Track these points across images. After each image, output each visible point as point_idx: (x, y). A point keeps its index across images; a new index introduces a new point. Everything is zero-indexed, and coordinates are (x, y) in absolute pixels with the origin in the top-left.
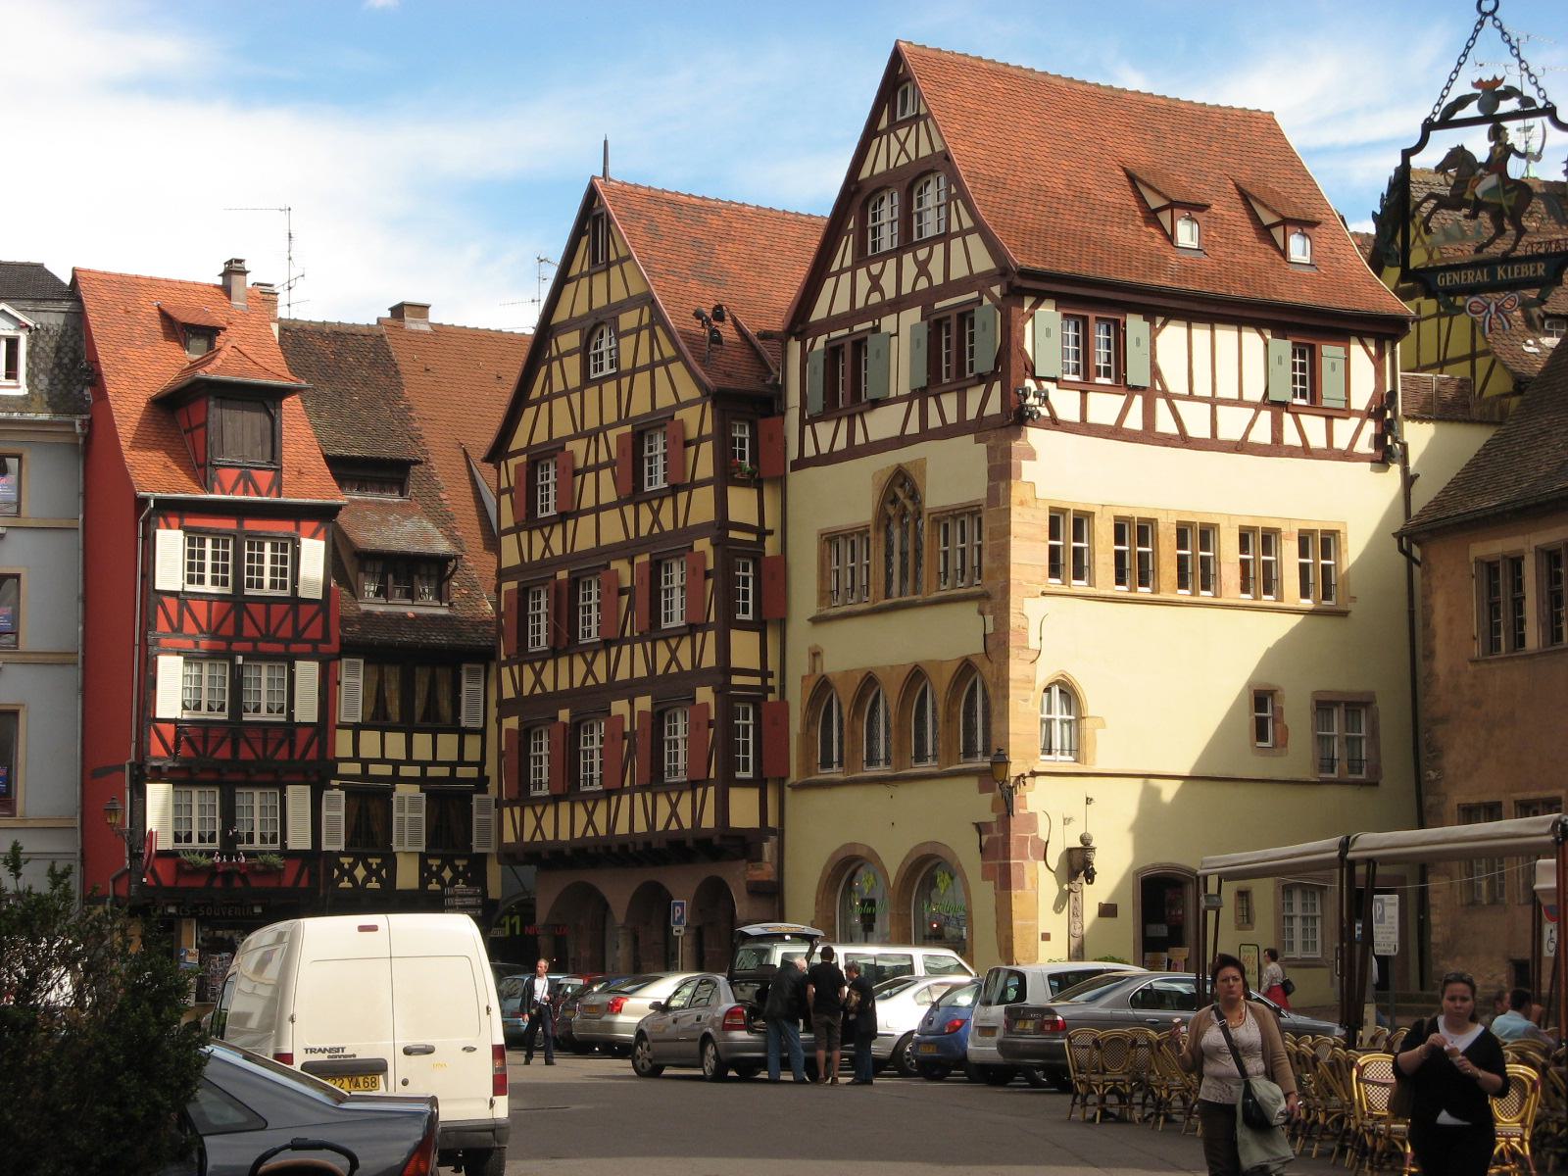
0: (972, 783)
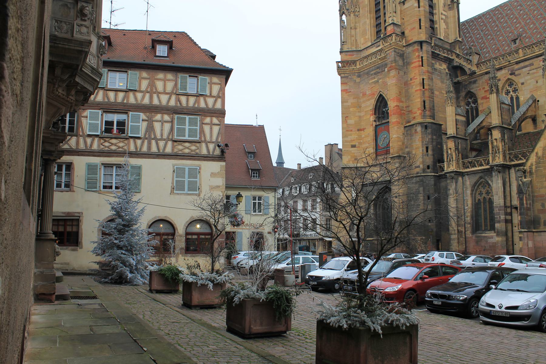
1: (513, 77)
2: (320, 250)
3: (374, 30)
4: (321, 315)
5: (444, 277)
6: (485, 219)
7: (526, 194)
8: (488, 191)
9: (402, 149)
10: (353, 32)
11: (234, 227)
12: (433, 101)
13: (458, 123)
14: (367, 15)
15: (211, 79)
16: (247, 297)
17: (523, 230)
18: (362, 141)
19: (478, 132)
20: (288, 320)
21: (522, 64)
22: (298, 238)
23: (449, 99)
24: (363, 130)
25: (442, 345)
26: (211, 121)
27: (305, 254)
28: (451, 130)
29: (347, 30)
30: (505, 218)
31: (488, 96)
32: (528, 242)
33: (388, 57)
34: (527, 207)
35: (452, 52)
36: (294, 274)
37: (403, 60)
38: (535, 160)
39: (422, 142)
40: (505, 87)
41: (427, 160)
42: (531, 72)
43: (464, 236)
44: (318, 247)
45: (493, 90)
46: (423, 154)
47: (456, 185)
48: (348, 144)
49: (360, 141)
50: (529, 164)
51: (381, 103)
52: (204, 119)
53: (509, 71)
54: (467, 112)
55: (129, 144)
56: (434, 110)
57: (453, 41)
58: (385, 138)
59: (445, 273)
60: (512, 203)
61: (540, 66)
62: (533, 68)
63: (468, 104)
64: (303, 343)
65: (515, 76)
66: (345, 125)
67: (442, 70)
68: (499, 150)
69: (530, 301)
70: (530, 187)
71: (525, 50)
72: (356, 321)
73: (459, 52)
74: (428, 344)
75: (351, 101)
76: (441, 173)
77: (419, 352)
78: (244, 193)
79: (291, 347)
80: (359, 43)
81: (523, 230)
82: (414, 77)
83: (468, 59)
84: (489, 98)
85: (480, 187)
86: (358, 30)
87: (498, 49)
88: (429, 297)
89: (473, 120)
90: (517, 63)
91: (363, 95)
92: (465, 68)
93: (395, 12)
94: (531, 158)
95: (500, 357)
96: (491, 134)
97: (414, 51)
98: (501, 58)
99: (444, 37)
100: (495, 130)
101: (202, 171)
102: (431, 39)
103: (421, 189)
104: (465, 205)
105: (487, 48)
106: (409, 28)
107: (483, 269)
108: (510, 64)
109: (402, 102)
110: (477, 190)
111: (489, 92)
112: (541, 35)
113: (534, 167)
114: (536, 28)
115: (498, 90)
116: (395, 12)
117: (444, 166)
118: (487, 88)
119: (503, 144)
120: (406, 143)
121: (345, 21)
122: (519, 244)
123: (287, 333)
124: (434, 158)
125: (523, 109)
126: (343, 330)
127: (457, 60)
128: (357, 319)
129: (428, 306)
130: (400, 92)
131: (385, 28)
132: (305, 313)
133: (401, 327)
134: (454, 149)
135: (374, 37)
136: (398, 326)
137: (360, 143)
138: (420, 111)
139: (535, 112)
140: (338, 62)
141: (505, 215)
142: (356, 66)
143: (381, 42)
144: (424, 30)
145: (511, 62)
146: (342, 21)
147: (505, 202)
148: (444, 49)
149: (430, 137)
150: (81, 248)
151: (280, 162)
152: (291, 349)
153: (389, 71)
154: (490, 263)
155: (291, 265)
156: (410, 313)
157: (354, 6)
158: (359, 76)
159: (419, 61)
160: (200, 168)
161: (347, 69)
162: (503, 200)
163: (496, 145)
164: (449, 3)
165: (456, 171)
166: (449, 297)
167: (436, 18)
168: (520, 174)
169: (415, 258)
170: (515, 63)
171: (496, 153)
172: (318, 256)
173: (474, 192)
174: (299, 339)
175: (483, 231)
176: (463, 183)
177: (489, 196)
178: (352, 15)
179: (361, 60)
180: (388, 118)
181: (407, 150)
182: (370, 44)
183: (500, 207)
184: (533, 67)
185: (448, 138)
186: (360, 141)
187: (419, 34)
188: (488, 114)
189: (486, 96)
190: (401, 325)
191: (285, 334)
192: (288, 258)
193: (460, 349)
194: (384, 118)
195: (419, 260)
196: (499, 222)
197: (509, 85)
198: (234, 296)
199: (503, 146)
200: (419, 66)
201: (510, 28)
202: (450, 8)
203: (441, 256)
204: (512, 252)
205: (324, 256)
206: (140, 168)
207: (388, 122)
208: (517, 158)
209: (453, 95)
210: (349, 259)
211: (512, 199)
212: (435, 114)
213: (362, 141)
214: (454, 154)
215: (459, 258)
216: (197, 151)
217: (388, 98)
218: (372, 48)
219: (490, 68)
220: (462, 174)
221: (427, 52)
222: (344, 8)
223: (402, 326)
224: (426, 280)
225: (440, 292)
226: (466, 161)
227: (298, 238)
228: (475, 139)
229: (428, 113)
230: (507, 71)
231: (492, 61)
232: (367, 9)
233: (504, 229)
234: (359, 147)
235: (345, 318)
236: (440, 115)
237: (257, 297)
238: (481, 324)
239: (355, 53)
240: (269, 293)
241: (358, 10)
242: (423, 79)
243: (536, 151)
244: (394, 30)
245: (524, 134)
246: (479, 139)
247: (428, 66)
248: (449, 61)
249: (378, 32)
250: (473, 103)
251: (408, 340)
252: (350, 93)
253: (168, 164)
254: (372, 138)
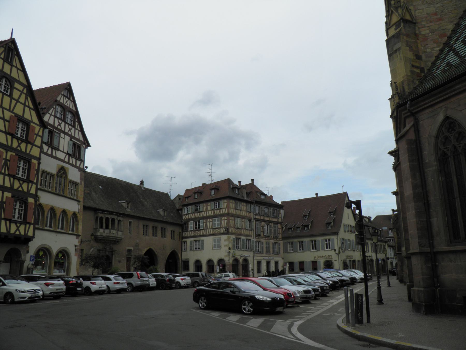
0: (75, 237)
15: (224, 201)
26: (224, 218)
52: (207, 220)
55: (200, 232)
101: (221, 240)
150: (189, 271)
160: (221, 238)
195: (151, 277)
206: (203, 241)
216: (220, 231)
253: (211, 238)
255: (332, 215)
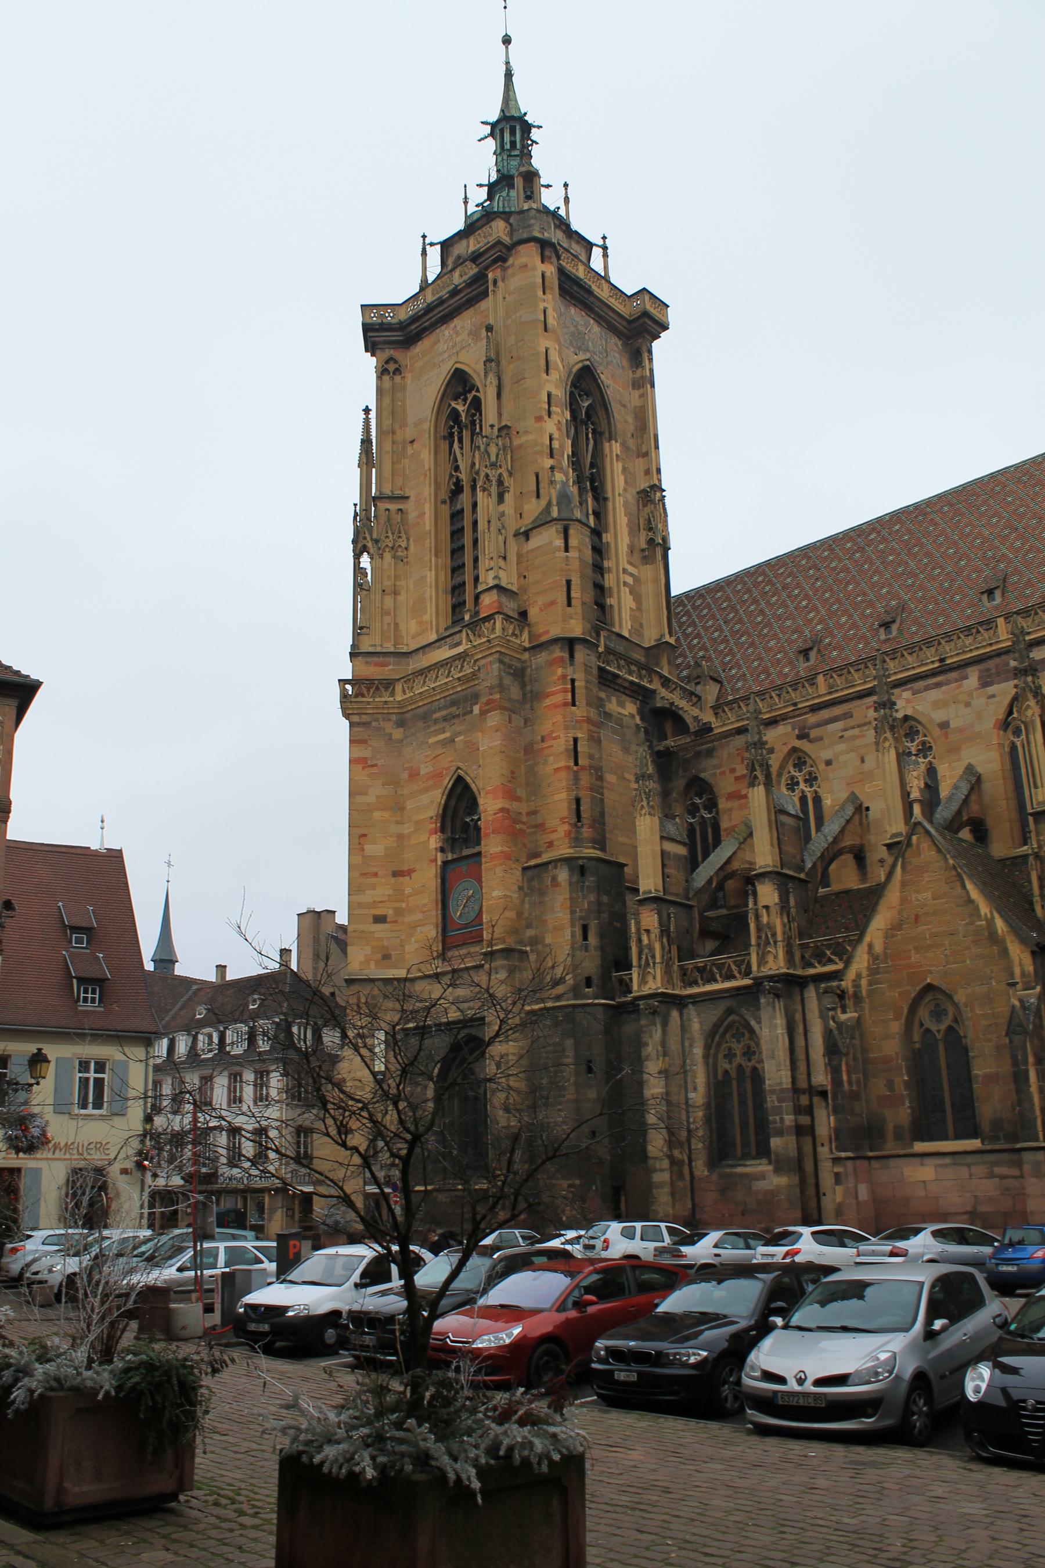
1: (803, 745)
2: (277, 1223)
3: (446, 602)
4: (295, 1439)
5: (641, 1299)
6: (744, 1125)
7: (847, 1054)
8: (749, 1047)
9: (515, 932)
10: (389, 601)
11: (17, 1153)
12: (602, 800)
13: (666, 862)
14: (427, 558)
16: (54, 1384)
17: (843, 1154)
18: (404, 905)
19: (720, 887)
20: (184, 1455)
21: (825, 714)
22: (210, 1187)
23: (644, 797)
24: (409, 873)
25: (649, 1508)
27: (235, 1238)
28: (649, 882)
29: (372, 597)
30: (796, 1120)
31: (743, 793)
32: (856, 1187)
33: (482, 674)
34: (851, 1091)
35: (651, 671)
36: (198, 1299)
37: (523, 686)
38: (865, 964)
39: (572, 912)
40: (786, 771)
41: (587, 964)
42: (847, 734)
43: (687, 1177)
44: (273, 1211)
45: (756, 777)
46: (573, 944)
47: (664, 1032)
48: (366, 911)
49: (398, 905)
50: (851, 974)
51: (459, 799)
53: (794, 729)
54: (691, 832)
56: (604, 824)
57: (653, 643)
58: (470, 897)
59: (645, 1287)
60: (813, 1079)
61: (867, 720)
62: (852, 725)
63: (693, 810)
64: (231, 1530)
65: (810, 741)
66: (358, 859)
67: (625, 719)
68: (774, 935)
69: (878, 1359)
70: (857, 1035)
71: (832, 677)
72: (403, 1455)
73: (670, 673)
74: (608, 1508)
75: (377, 791)
76: (623, 999)
77: (589, 1537)
78: (53, 1051)
79: (192, 1546)
80: (404, 633)
81: (843, 1154)
82: (552, 732)
83: (692, 693)
84: (745, 797)
85: (728, 1036)
86: (402, 598)
87: (766, 671)
88: (601, 1361)
89: (706, 855)
90: (815, 709)
91: (411, 776)
92: (685, 716)
93: (505, 558)
94: (856, 959)
95: (810, 1534)
96: (755, 894)
97: (551, 663)
98: (773, 694)
99: (630, 631)
100: (763, 883)
102: (598, 635)
103: (569, 1043)
104: (690, 1086)
105: (740, 667)
106: (541, 600)
107: (745, 1270)
108: (797, 712)
109: (518, 799)
110: (719, 1045)
111: (747, 781)
112: (867, 643)
113: (864, 982)
114: (854, 625)
115: (768, 776)
116: (505, 558)
117: (631, 979)
118: (742, 770)
119: (786, 920)
120: (526, 915)
121: (369, 572)
122: (834, 1195)
123: (182, 1498)
124: (603, 957)
125: (832, 828)
126: (364, 1484)
127: (663, 692)
128: (404, 1448)
129: (599, 1387)
130: (513, 772)
131: (477, 597)
132: (235, 1428)
133: (536, 1466)
134: (657, 931)
135: (445, 621)
136: (526, 1462)
137: (399, 912)
138: (566, 827)
139: (861, 838)
140: (342, 682)
141: (795, 1114)
142: (392, 694)
143: (464, 633)
144: (579, 610)
145: (800, 706)
146: (358, 570)
147: (793, 1078)
148: (630, 662)
149: (592, 898)
151: (166, 959)
152: (194, 1553)
153: (483, 713)
154: (762, 1253)
155: (192, 1273)
156: (558, 1419)
157: (393, 534)
158: (401, 723)
159: (565, 691)
161: (368, 703)
162: (789, 1073)
163: (768, 923)
164: (644, 545)
165: (663, 994)
166: (659, 1359)
167: (609, 581)
168: (829, 1001)
169: (555, 1243)
170: (807, 710)
171: (768, 943)
172: (274, 1244)
173: (712, 1052)
174: (218, 1517)
175: (739, 1159)
176: (682, 1026)
177: (753, 1062)
178: (388, 556)
179: (410, 679)
180: (478, 843)
181: (530, 933)
182: (433, 637)
183: (782, 1090)
184: (850, 722)
185: (642, 902)
186: (398, 905)
187: (566, 618)
188: (745, 840)
189: (739, 791)
190: (534, 1460)
191: (173, 1504)
192: (180, 1250)
193: (701, 1518)
194: (466, 842)
195: (568, 1247)
196: (780, 1133)
197: (795, 766)
198: (13, 1385)
199: (784, 926)
200: (566, 704)
201: (794, 619)
202: (644, 557)
203: (629, 1234)
204: (816, 1217)
205: (292, 1243)
207: (479, 854)
208: (820, 957)
209: (652, 785)
210: (365, 1252)
211: (812, 1069)
212: (607, 835)
213: (404, 905)
214: (657, 946)
215: (676, 1239)
217: (481, 786)
218: (439, 648)
219: (748, 719)
220: (679, 1002)
221: (587, 669)
222: (367, 535)
223: (539, 1463)
224: (591, 1309)
225: (632, 1343)
226: (689, 964)
227: (210, 1187)
228: (713, 905)
229: (586, 832)
230: (789, 728)
231: (751, 701)
232: (429, 543)
233: (793, 1153)
234: (395, 922)
235: (368, 1446)
236: (620, 839)
237: (89, 1383)
238: (750, 1432)
239: (391, 660)
240: (127, 1370)
241: (404, 545)
242: (575, 740)
243: (867, 939)
244: (500, 605)
245: (838, 894)
246: (721, 907)
247: (589, 704)
248: (642, 695)
249: (457, 607)
250: (706, 808)
251: (556, 1504)
252: (375, 770)
254: (434, 897)
255: (79, 941)
